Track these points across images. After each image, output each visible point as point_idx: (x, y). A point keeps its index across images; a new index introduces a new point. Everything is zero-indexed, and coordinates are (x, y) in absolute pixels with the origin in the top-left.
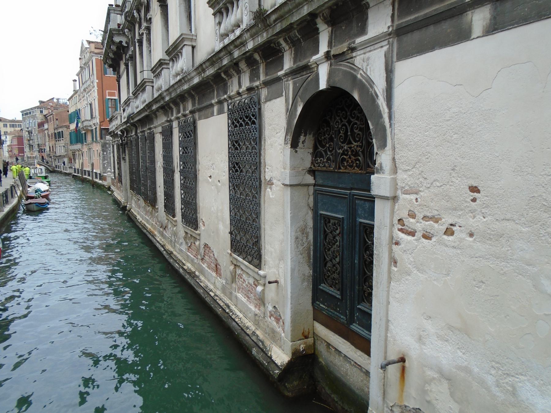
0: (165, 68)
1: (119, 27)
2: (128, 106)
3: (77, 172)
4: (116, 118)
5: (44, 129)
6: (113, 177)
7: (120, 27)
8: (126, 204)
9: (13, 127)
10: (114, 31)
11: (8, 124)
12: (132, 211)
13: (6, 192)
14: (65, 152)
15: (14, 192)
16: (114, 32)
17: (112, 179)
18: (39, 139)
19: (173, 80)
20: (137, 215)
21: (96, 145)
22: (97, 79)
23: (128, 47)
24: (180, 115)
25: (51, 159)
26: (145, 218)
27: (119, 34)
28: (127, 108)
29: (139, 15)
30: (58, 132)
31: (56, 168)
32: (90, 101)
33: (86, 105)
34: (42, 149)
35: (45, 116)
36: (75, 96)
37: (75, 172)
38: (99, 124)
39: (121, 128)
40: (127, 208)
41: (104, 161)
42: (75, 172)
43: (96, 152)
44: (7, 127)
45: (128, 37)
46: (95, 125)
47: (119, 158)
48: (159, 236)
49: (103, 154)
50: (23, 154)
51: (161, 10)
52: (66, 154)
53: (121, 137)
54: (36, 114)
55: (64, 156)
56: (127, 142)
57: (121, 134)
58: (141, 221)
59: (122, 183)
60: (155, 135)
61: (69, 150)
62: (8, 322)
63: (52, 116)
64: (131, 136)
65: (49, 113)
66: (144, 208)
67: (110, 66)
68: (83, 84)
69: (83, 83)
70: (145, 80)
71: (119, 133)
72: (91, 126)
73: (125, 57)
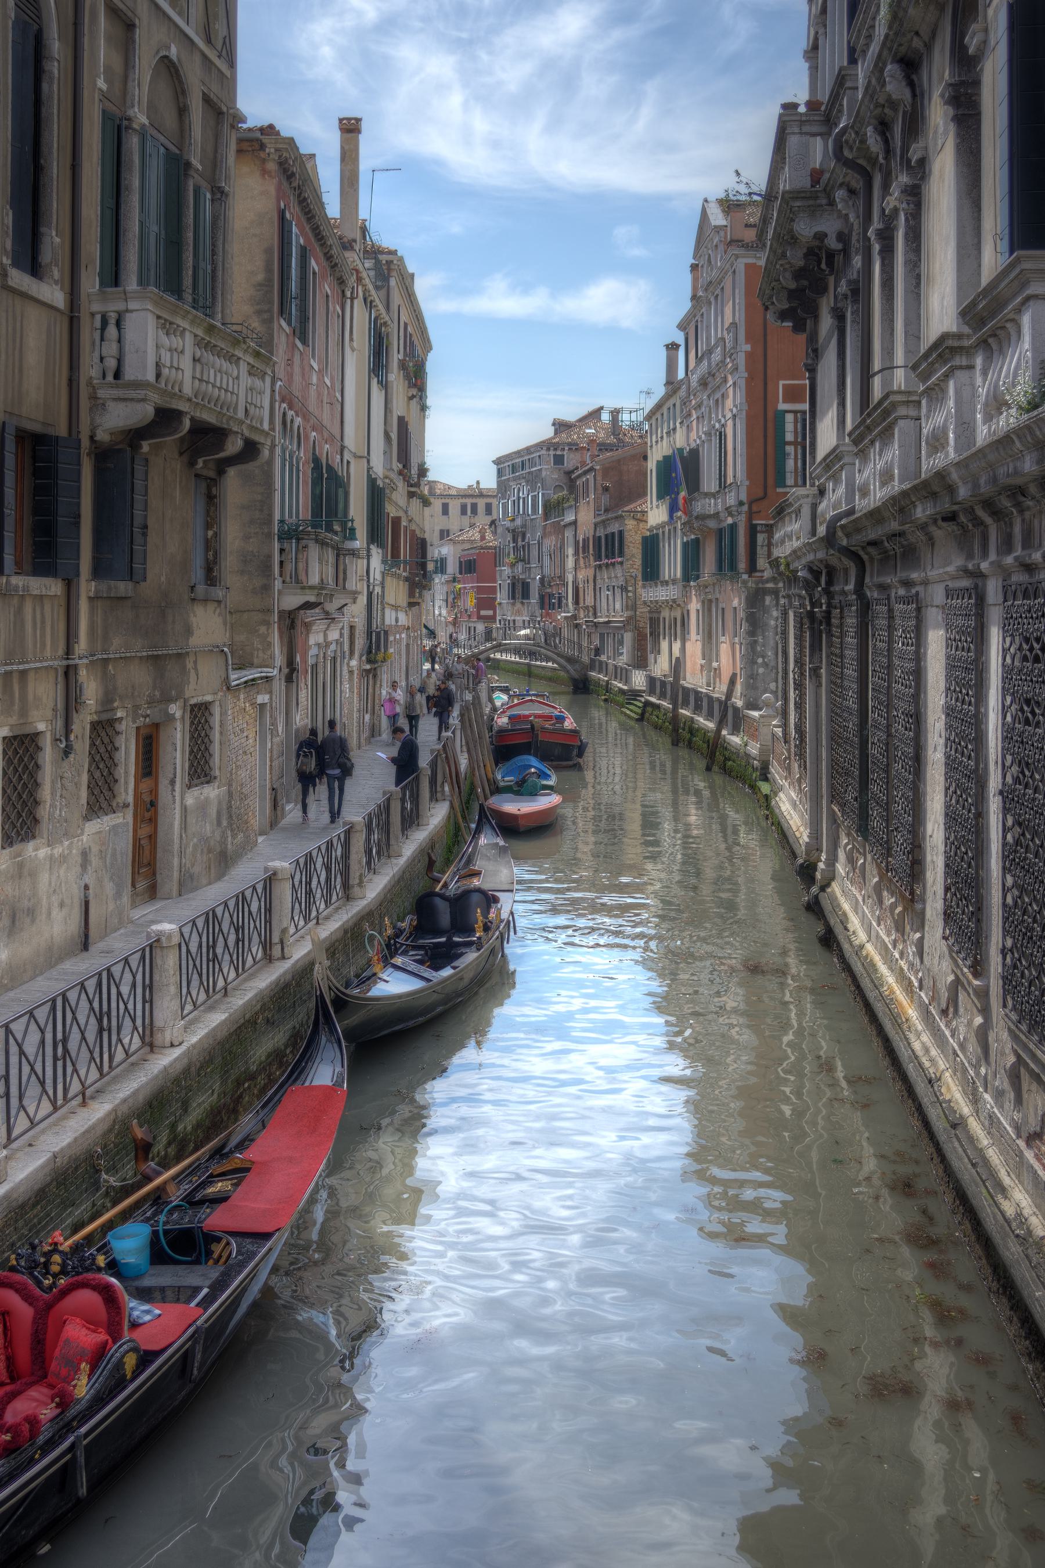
0: (961, 368)
2: (835, 478)
3: (658, 691)
5: (562, 523)
6: (779, 731)
7: (818, 182)
12: (833, 892)
14: (627, 609)
16: (798, 204)
18: (546, 560)
19: (984, 424)
22: (748, 339)
23: (846, 251)
24: (1009, 560)
25: (579, 633)
26: (878, 936)
27: (814, 211)
29: (886, 142)
30: (606, 536)
34: (551, 596)
35: (569, 473)
36: (670, 403)
48: (920, 1028)
50: (490, 613)
51: (958, 135)
53: (809, 586)
54: (540, 470)
58: (862, 947)
60: (923, 609)
63: (590, 477)
65: (583, 463)
67: (783, 316)
68: (699, 360)
69: (700, 355)
70: (894, 398)
73: (835, 290)
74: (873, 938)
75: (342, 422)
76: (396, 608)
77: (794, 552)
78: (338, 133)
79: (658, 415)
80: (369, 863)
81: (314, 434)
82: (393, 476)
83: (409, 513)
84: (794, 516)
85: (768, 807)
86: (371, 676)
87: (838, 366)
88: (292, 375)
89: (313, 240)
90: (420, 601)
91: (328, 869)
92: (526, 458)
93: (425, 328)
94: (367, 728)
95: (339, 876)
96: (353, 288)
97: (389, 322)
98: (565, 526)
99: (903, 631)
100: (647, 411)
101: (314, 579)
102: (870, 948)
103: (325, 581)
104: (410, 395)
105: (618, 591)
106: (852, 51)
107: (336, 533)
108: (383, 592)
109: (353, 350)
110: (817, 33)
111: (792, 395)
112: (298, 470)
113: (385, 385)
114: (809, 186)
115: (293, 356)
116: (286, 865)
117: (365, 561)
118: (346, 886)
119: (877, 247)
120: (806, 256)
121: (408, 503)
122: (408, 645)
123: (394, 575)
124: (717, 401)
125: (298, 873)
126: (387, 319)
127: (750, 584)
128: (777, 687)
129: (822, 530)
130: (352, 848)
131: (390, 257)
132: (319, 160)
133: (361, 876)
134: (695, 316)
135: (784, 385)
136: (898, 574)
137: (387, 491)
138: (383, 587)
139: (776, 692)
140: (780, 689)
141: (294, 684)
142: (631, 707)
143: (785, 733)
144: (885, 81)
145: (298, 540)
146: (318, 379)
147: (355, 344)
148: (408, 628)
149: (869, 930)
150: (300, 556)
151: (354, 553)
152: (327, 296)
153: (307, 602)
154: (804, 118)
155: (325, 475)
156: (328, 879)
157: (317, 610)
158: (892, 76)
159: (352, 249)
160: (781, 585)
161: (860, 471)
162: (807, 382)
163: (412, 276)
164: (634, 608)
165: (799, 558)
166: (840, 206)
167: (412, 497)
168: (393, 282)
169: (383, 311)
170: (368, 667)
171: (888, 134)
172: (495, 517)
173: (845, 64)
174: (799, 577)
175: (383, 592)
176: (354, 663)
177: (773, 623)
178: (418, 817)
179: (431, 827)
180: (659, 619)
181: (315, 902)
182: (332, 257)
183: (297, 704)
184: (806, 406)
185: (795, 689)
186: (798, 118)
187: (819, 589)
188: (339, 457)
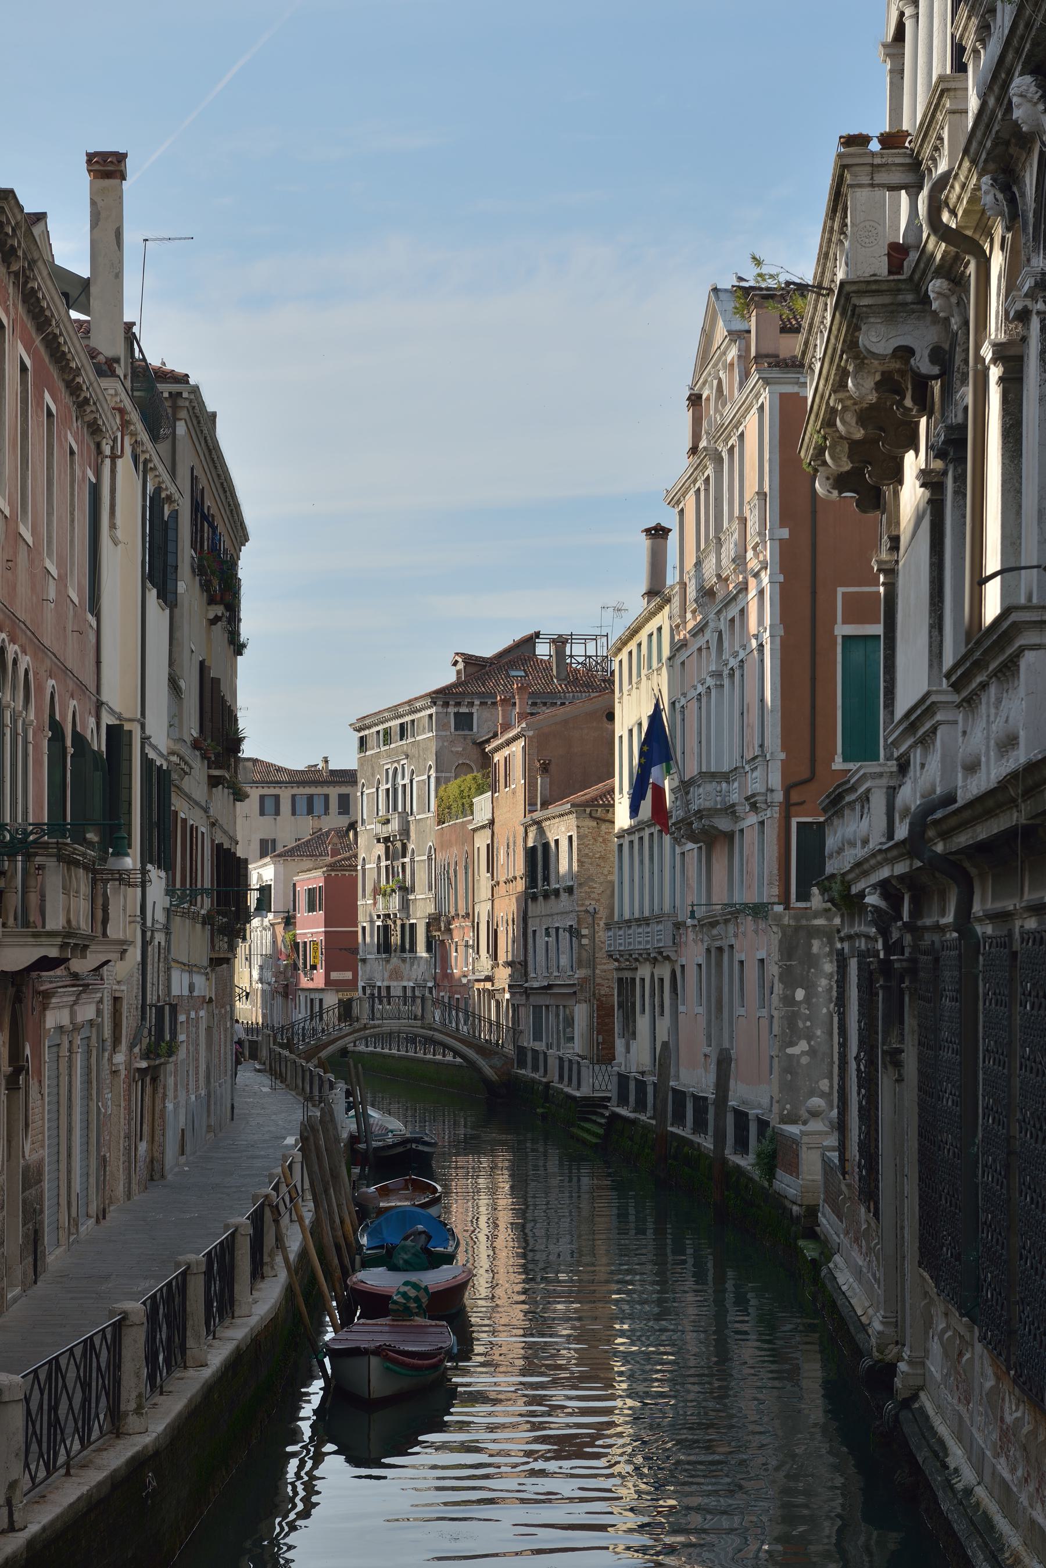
1: (895, 267)
2: (926, 741)
3: (632, 1098)
4: (859, 798)
6: (834, 1156)
8: (892, 1351)
9: (310, 811)
10: (861, 293)
11: (285, 795)
12: (922, 1409)
13: (228, 1248)
15: (269, 1240)
16: (866, 301)
17: (826, 1163)
20: (951, 1443)
21: (756, 932)
26: (994, 1473)
27: (893, 313)
28: (917, 756)
31: (522, 1064)
32: (735, 655)
33: (710, 682)
37: (623, 1100)
38: (779, 796)
39: (885, 873)
40: (898, 1382)
41: (792, 1044)
42: (623, 1100)
43: (752, 973)
44: (277, 813)
45: (947, 320)
46: (754, 807)
47: (867, 1042)
49: (788, 1000)
50: (348, 975)
52: (585, 980)
53: (883, 921)
55: (573, 994)
56: (913, 961)
57: (882, 904)
58: (968, 1492)
59: (877, 1209)
61: (601, 955)
62: (451, 1395)
64: (939, 928)
66: (993, 1399)
71: (872, 899)
72: (730, 810)
74: (987, 1478)
75: (98, 663)
76: (189, 968)
77: (858, 864)
78: (86, 178)
79: (632, 646)
80: (151, 1378)
81: (52, 682)
82: (186, 751)
83: (212, 812)
84: (858, 807)
85: (816, 1280)
86: (148, 1079)
87: (932, 565)
88: (14, 588)
89: (47, 359)
90: (230, 956)
91: (86, 1385)
92: (408, 719)
93: (237, 506)
94: (141, 1164)
95: (103, 1399)
96: (115, 440)
97: (177, 496)
98: (474, 830)
99: (1033, 985)
100: (613, 639)
101: (55, 922)
102: (980, 1492)
103: (74, 923)
104: (211, 616)
105: (564, 936)
106: (959, 50)
107: (90, 844)
108: (168, 941)
109: (116, 542)
110: (902, 14)
111: (857, 610)
112: (26, 742)
113: (168, 597)
114: (884, 271)
115: (15, 554)
116: (17, 1379)
117: (139, 890)
118: (116, 1415)
119: (995, 373)
120: (878, 386)
121: (210, 793)
122: (209, 1029)
123: (185, 914)
124: (732, 620)
125: (36, 1392)
126: (173, 489)
127: (786, 921)
128: (831, 1087)
129: (902, 832)
130: (124, 1352)
131: (175, 388)
132: (52, 224)
133: (140, 1396)
134: (695, 481)
135: (844, 594)
136: (1026, 897)
137: (174, 776)
138: (168, 934)
139: (831, 1094)
140: (836, 1087)
141: (22, 1092)
142: (587, 1125)
143: (842, 1159)
144: (1010, 102)
145: (28, 857)
146: (58, 592)
147: (119, 533)
148: (211, 1000)
149: (979, 1464)
150: (32, 882)
151: (122, 878)
152: (72, 452)
153: (45, 957)
154: (877, 161)
155: (71, 751)
156: (86, 1400)
157: (59, 972)
158: (1021, 96)
159: (113, 374)
160: (837, 921)
161: (964, 733)
162: (882, 589)
163: (214, 415)
164: (592, 964)
165: (866, 874)
166: (935, 306)
167: (215, 786)
168: (181, 428)
169: (166, 476)
170: (144, 1064)
171: (1015, 189)
172: (353, 819)
173: (948, 72)
174: (866, 905)
175: (168, 941)
176: (120, 1058)
177: (824, 982)
178: (232, 1305)
179: (253, 1320)
180: (633, 980)
181: (64, 1441)
182: (79, 387)
183: (27, 1125)
184: (878, 629)
185: (859, 1087)
186: (869, 160)
187: (900, 923)
188: (92, 721)
